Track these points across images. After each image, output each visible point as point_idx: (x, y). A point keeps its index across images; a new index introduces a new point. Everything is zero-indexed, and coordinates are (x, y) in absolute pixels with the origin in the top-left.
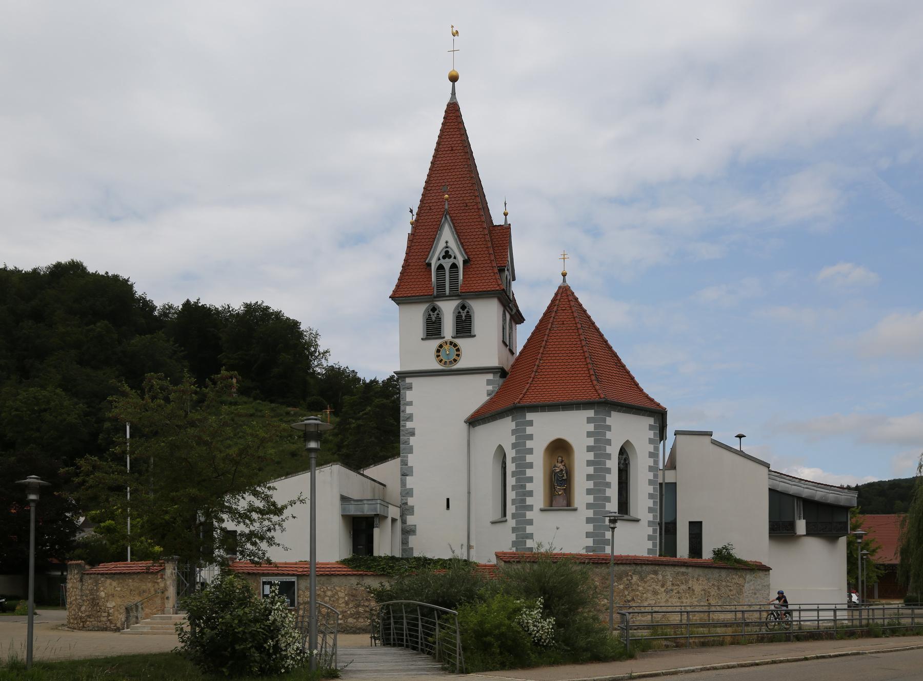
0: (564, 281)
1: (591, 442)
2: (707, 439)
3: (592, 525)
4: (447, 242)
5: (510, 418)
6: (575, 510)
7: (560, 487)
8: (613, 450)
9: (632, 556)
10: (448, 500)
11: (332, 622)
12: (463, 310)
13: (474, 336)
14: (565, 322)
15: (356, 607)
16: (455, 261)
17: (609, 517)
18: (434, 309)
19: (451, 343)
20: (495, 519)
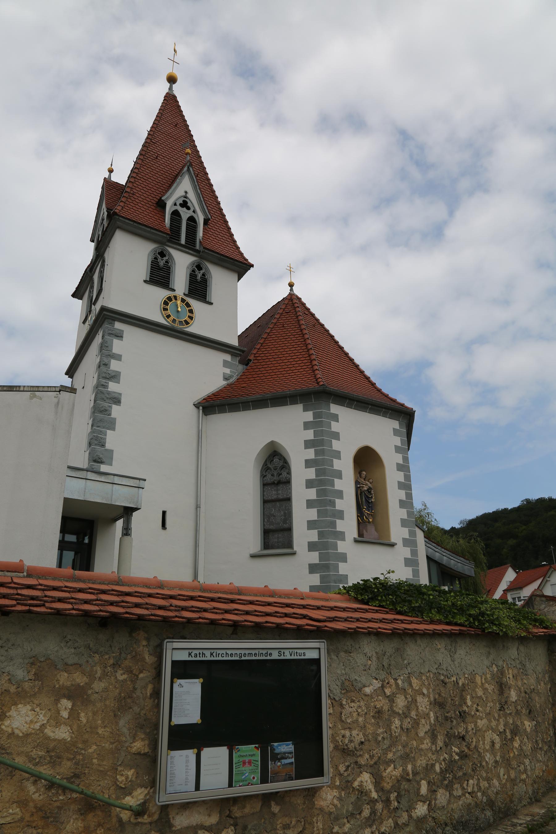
5: (300, 407)
10: (164, 513)
18: (162, 254)
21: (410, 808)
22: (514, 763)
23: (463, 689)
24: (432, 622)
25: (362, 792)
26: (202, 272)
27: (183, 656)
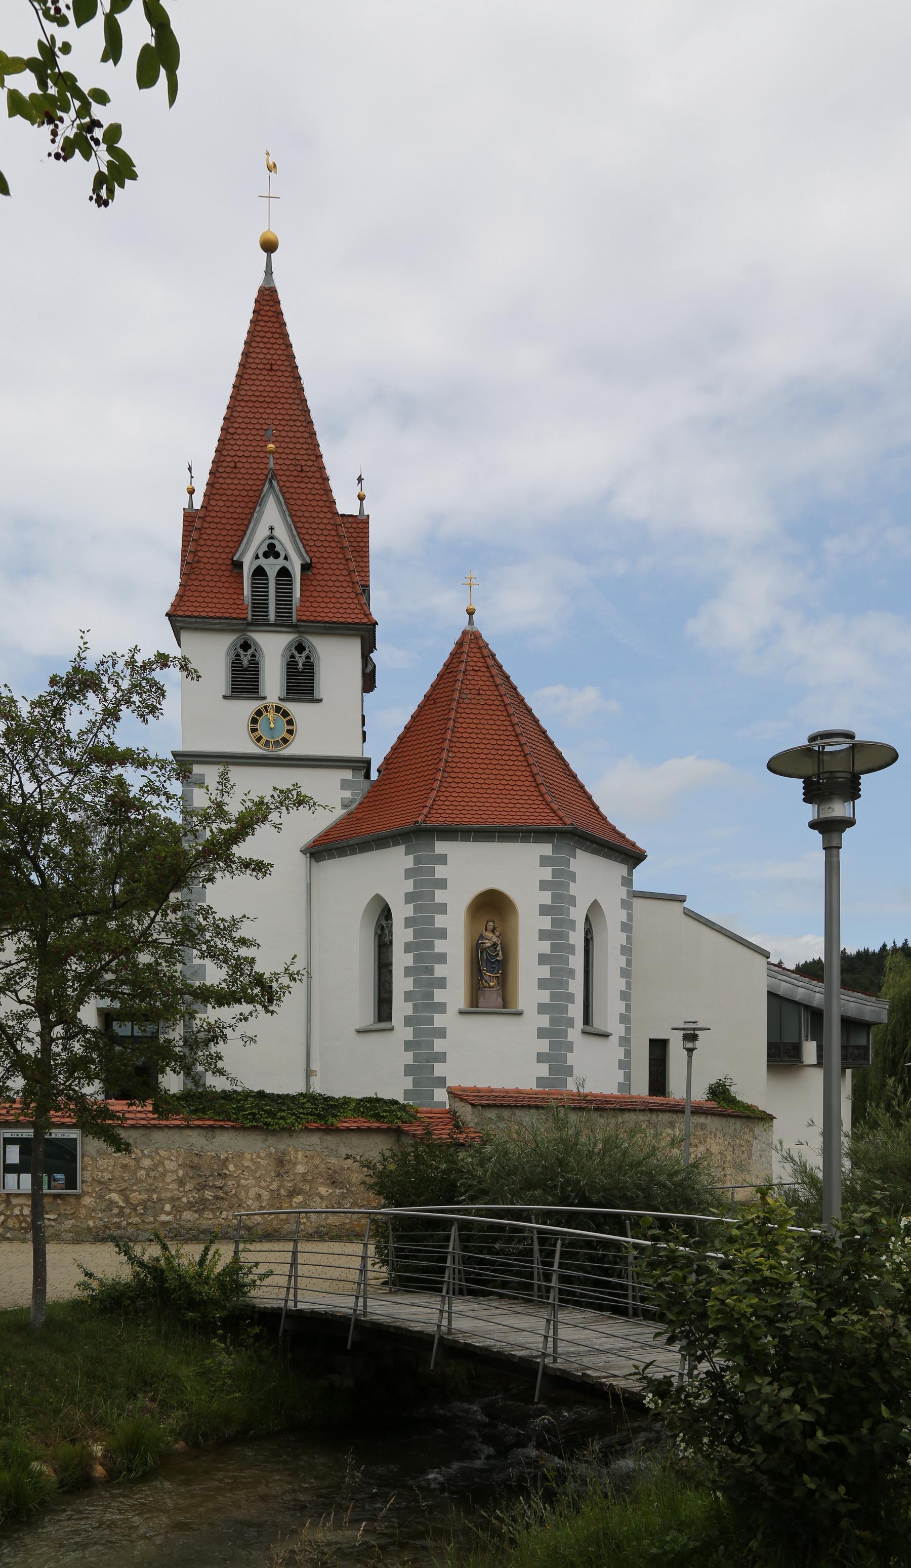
0: (471, 622)
1: (546, 898)
2: (676, 907)
3: (548, 1040)
4: (271, 529)
5: (401, 849)
6: (520, 1014)
7: (492, 972)
8: (578, 914)
9: (499, 1091)
11: (151, 1219)
12: (300, 652)
13: (319, 701)
14: (481, 692)
15: (199, 1190)
17: (684, 1029)
18: (246, 646)
19: (278, 709)
20: (359, 1026)
26: (304, 654)
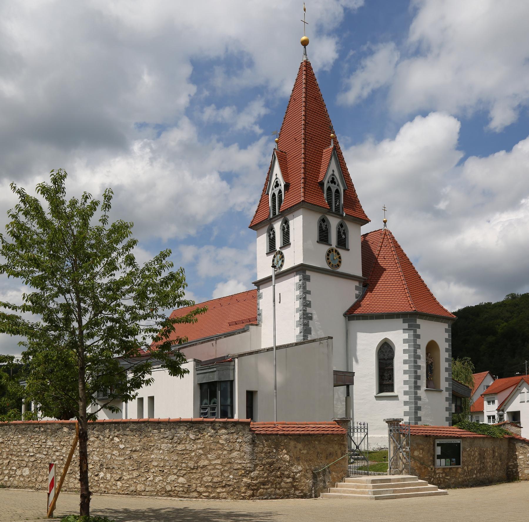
4: (333, 171)
5: (401, 320)
16: (338, 188)
21: (472, 476)
22: (495, 471)
23: (485, 451)
24: (479, 434)
25: (465, 470)
27: (438, 442)
